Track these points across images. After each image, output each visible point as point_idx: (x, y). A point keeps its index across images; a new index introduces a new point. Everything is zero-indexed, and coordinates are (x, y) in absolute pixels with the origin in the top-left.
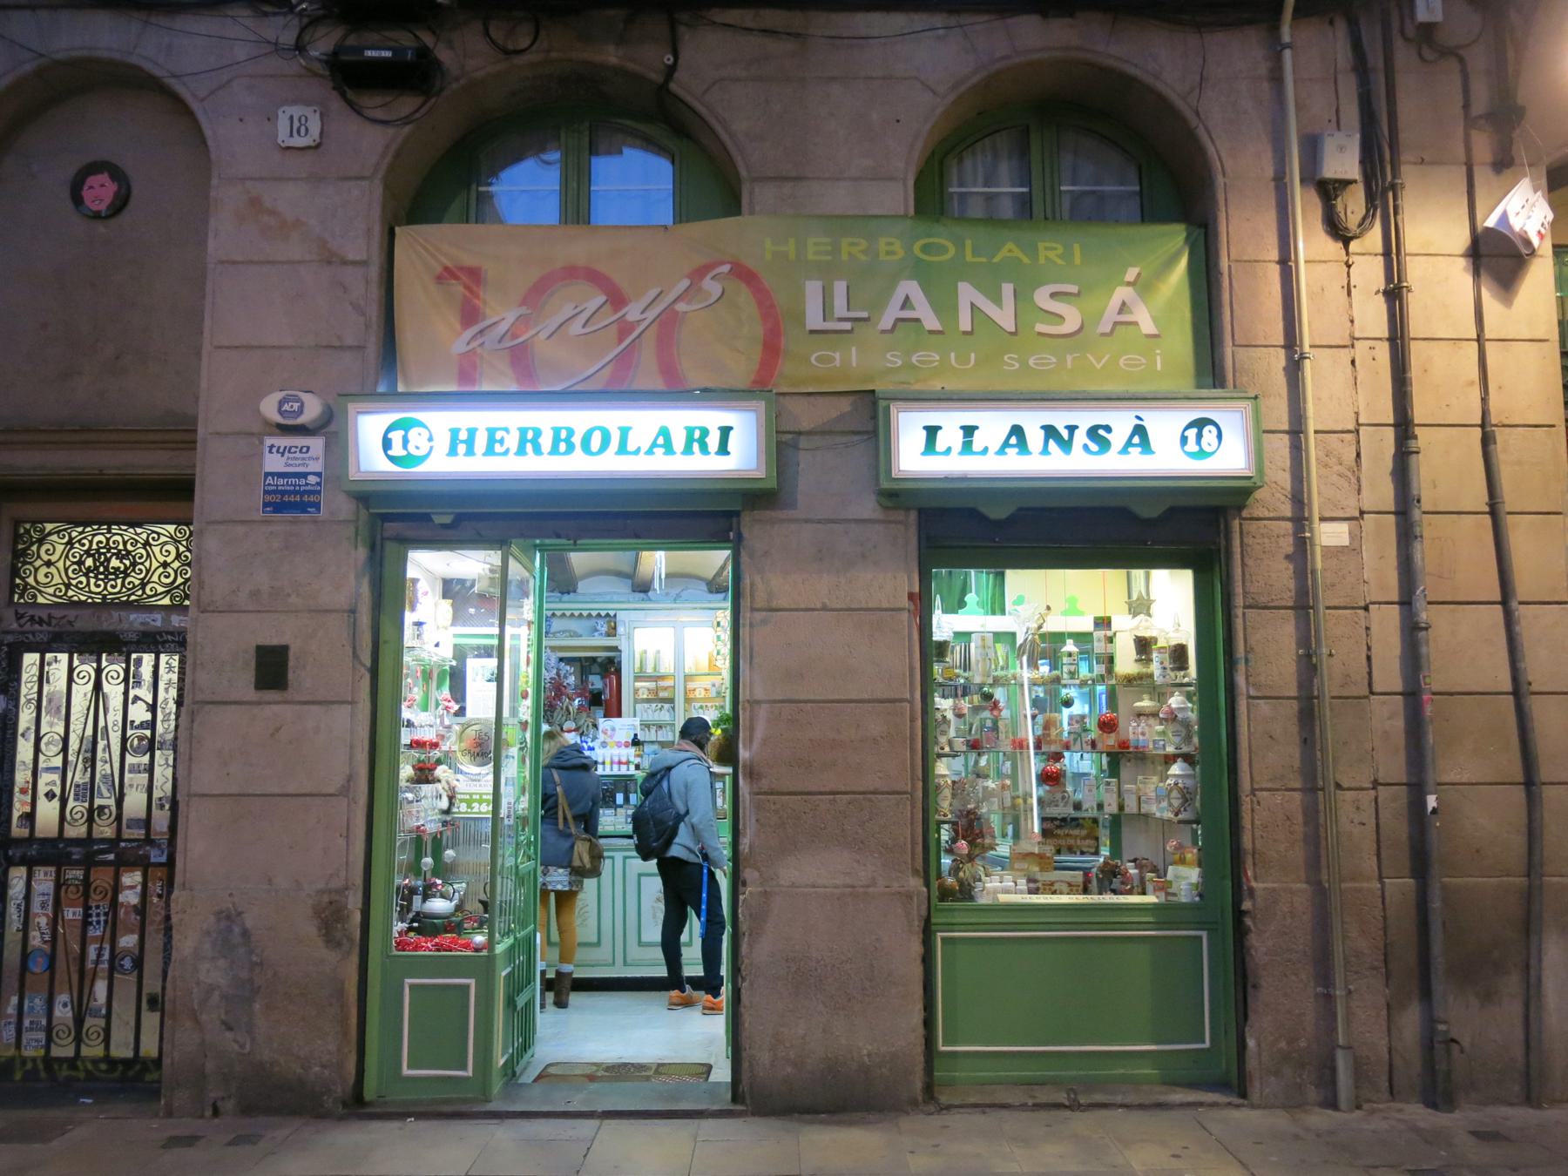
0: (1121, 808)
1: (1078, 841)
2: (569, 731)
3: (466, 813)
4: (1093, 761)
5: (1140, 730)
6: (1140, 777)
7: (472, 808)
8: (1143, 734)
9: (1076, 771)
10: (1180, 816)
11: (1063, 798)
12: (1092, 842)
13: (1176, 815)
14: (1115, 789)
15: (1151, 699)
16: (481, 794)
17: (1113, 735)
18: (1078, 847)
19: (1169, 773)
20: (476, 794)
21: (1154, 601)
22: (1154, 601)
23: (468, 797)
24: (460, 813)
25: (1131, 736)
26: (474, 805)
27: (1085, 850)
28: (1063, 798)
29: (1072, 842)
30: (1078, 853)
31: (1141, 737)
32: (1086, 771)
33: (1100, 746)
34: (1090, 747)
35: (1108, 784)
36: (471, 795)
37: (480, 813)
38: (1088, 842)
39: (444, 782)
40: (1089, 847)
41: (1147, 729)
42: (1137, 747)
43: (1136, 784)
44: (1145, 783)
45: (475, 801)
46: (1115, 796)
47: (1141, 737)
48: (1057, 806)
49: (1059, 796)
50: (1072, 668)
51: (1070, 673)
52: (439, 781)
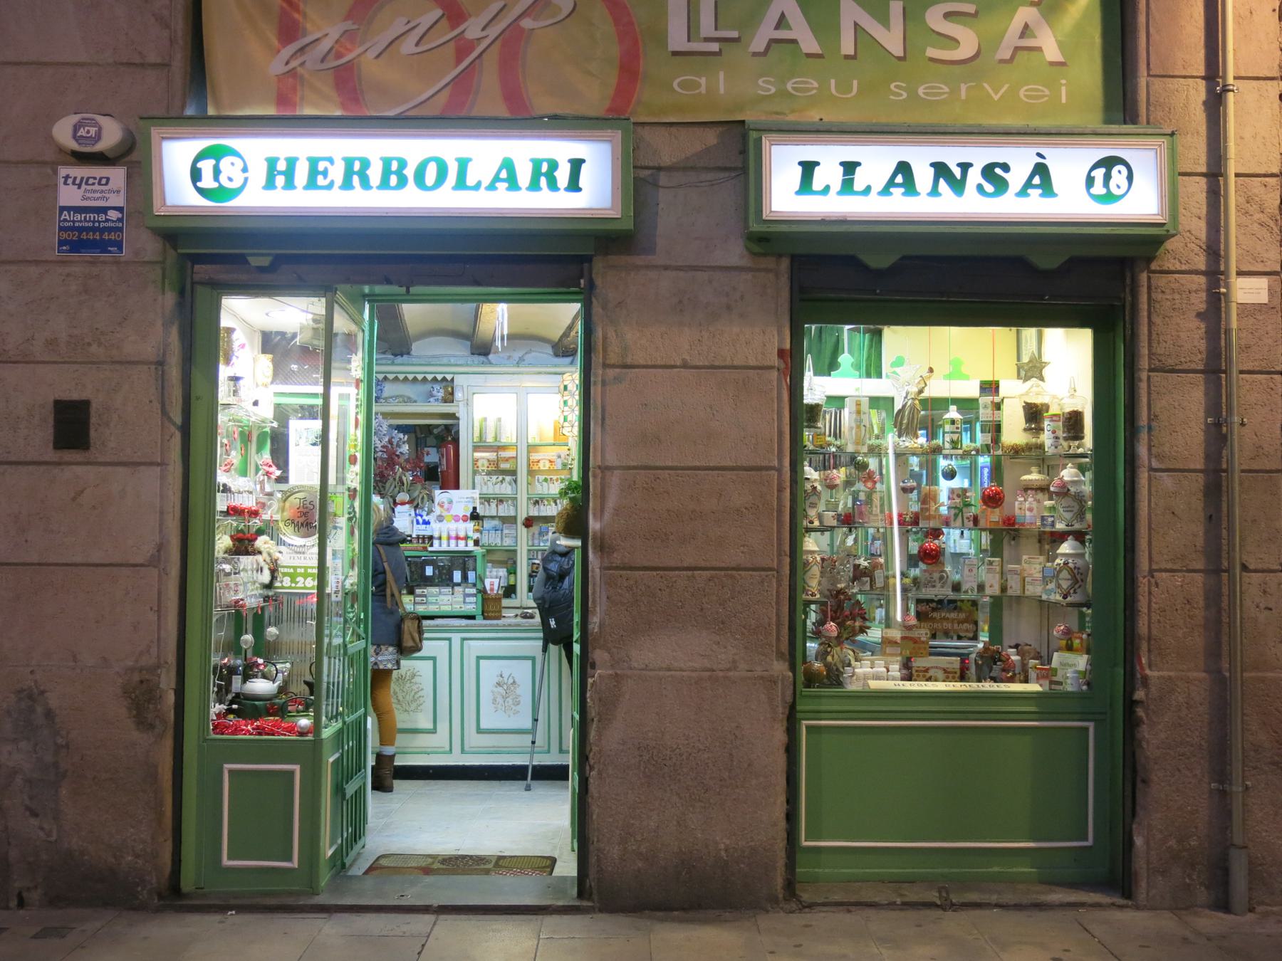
1: (956, 625)
2: (403, 504)
3: (290, 587)
4: (972, 540)
5: (1027, 504)
7: (297, 583)
8: (1031, 510)
11: (941, 578)
12: (971, 627)
13: (1065, 597)
14: (998, 569)
15: (1040, 472)
16: (306, 568)
17: (997, 510)
18: (955, 631)
19: (1058, 551)
20: (301, 567)
23: (292, 570)
24: (283, 587)
25: (1017, 512)
26: (300, 579)
27: (961, 634)
28: (941, 578)
29: (949, 626)
30: (955, 637)
31: (1028, 513)
33: (982, 523)
36: (295, 568)
37: (305, 588)
38: (966, 626)
39: (265, 555)
40: (967, 631)
41: (1035, 505)
45: (301, 575)
46: (998, 576)
47: (1028, 513)
48: (934, 586)
49: (936, 576)
50: (955, 437)
52: (260, 553)
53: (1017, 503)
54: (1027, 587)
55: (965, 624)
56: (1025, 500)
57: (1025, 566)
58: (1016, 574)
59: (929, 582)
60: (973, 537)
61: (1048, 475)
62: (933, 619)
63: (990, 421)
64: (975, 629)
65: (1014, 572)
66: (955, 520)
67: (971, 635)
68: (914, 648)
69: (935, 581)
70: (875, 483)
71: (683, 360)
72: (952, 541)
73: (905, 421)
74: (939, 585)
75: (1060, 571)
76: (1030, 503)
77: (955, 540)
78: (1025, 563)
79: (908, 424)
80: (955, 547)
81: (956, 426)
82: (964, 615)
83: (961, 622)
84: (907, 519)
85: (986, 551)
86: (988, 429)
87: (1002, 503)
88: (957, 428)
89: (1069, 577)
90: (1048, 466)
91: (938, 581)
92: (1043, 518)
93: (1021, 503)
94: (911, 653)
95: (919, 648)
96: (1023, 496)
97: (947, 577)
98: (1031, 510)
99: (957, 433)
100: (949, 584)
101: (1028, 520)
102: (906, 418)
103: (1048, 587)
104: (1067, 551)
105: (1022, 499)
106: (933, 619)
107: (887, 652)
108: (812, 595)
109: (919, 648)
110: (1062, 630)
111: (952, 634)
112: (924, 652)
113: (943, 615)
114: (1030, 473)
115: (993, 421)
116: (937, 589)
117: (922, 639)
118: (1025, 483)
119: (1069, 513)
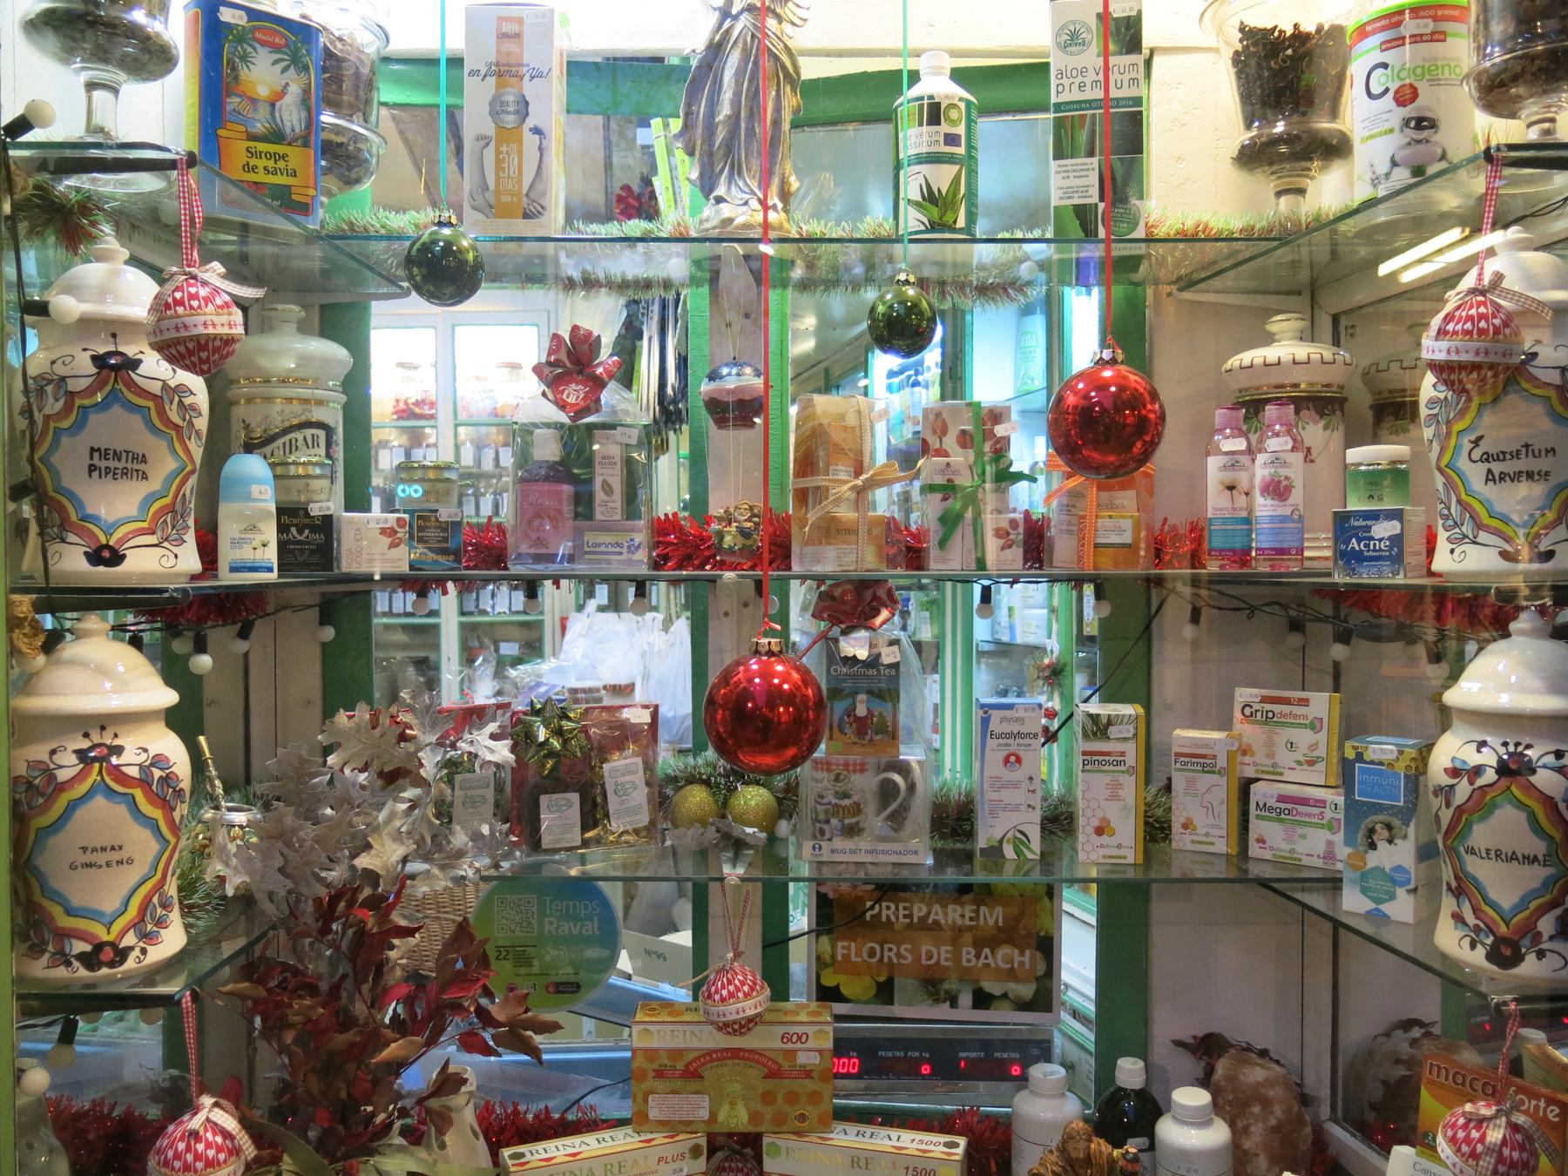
0: (1156, 829)
1: (968, 953)
4: (1053, 610)
5: (1261, 470)
6: (1244, 694)
8: (1278, 490)
9: (1005, 639)
10: (1530, 967)
11: (887, 792)
12: (1027, 959)
13: (1505, 954)
14: (1132, 753)
15: (1309, 335)
17: (1127, 499)
18: (965, 975)
19: (1452, 697)
21: (1296, 26)
22: (1296, 26)
25: (1216, 502)
27: (992, 987)
28: (887, 792)
29: (943, 954)
30: (966, 999)
31: (1264, 507)
32: (1032, 640)
33: (1063, 551)
34: (1017, 553)
35: (1098, 728)
38: (1005, 955)
40: (1011, 975)
41: (1295, 469)
42: (1242, 557)
43: (1226, 725)
44: (1268, 719)
46: (1129, 786)
47: (1264, 507)
48: (851, 831)
49: (864, 784)
50: (942, 176)
51: (931, 197)
53: (1213, 463)
54: (1257, 827)
55: (1004, 951)
56: (1251, 452)
57: (1248, 732)
58: (1209, 770)
59: (836, 810)
60: (1056, 602)
61: (1336, 342)
62: (881, 929)
63: (1089, 104)
64: (1041, 969)
65: (1200, 759)
66: (942, 544)
67: (1026, 991)
68: (768, 1098)
69: (857, 809)
70: (598, 384)
71: (584, 272)
72: (1005, 611)
73: (725, 110)
74: (875, 822)
75: (1481, 803)
76: (1277, 461)
77: (1010, 609)
78: (1249, 718)
79: (735, 119)
80: (1012, 628)
81: (945, 128)
82: (999, 910)
83: (992, 940)
84: (728, 541)
85: (1091, 639)
86: (1083, 138)
87: (1146, 455)
88: (951, 139)
89: (1539, 847)
90: (1336, 319)
91: (870, 807)
92: (1343, 525)
93: (1233, 458)
94: (754, 1117)
95: (792, 1098)
96: (1240, 433)
97: (912, 788)
98: (1278, 490)
99: (950, 159)
100: (920, 813)
101: (1262, 540)
102: (727, 96)
103: (1372, 859)
104: (1504, 701)
105: (1240, 444)
106: (881, 929)
107: (654, 1114)
108: (91, 960)
109: (792, 1098)
110: (1496, 1151)
111: (950, 985)
112: (813, 1112)
113: (919, 910)
114: (1269, 339)
115: (1106, 102)
116: (863, 843)
117: (802, 1059)
118: (1245, 381)
119: (1523, 489)
